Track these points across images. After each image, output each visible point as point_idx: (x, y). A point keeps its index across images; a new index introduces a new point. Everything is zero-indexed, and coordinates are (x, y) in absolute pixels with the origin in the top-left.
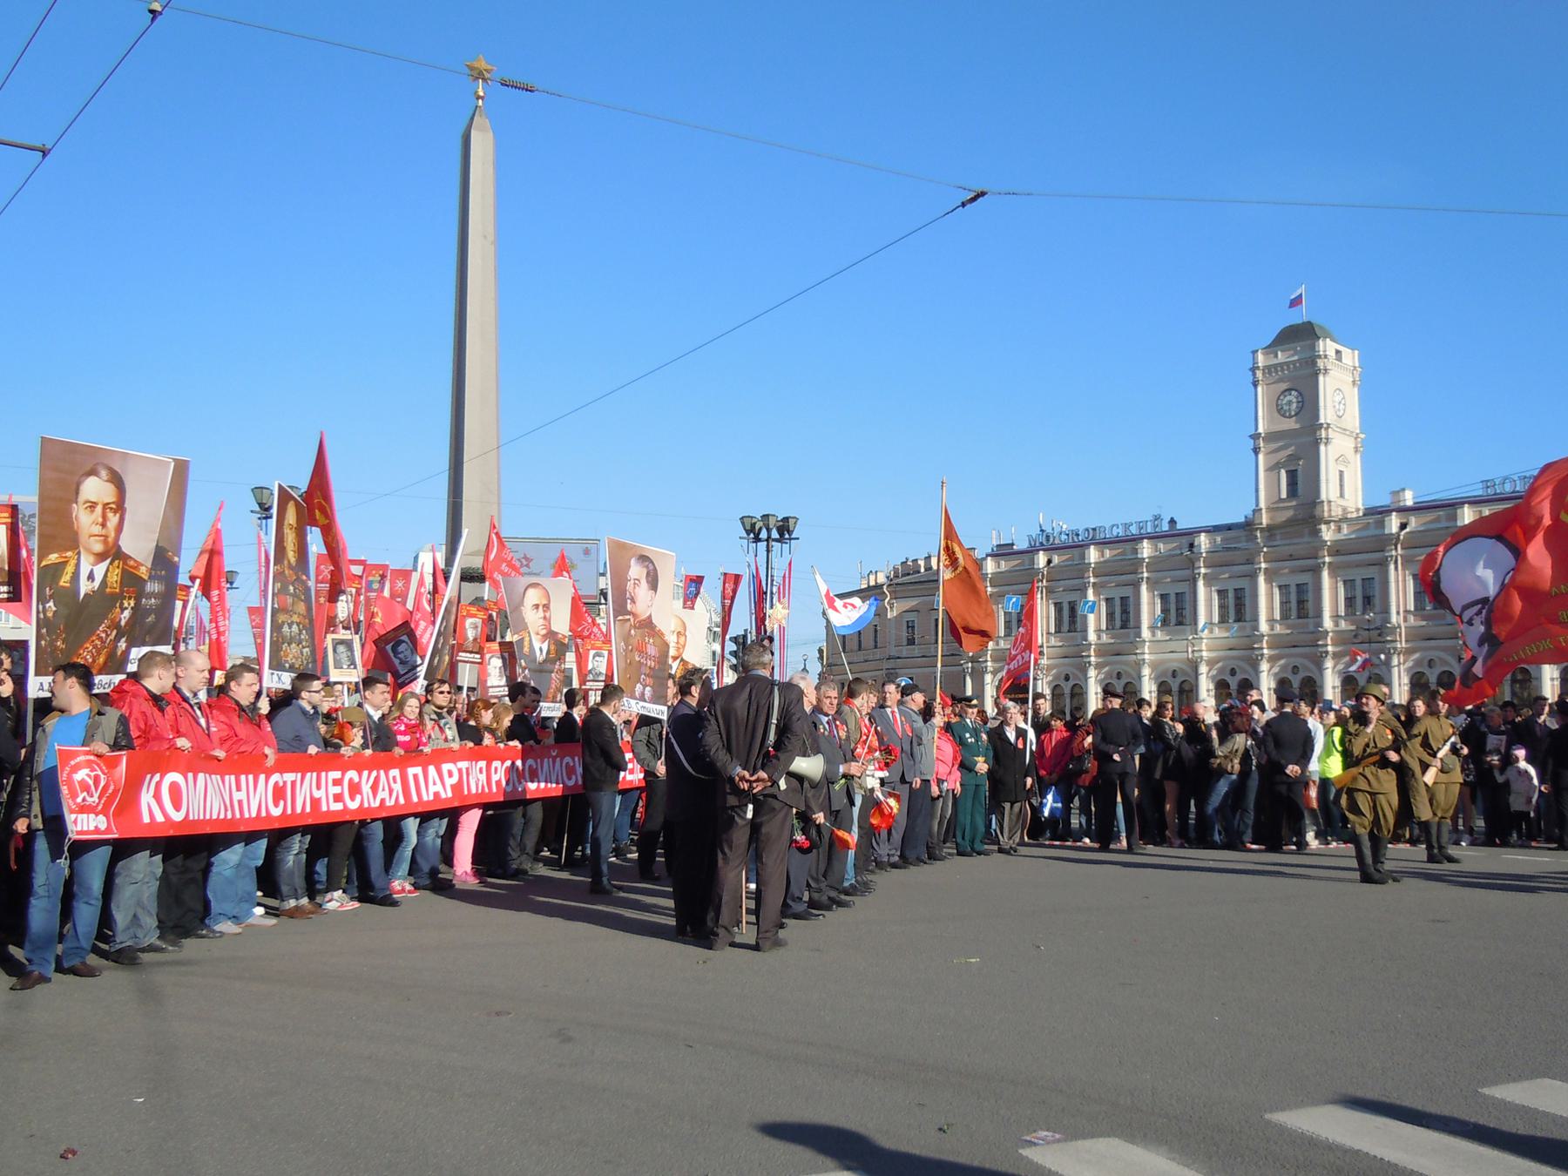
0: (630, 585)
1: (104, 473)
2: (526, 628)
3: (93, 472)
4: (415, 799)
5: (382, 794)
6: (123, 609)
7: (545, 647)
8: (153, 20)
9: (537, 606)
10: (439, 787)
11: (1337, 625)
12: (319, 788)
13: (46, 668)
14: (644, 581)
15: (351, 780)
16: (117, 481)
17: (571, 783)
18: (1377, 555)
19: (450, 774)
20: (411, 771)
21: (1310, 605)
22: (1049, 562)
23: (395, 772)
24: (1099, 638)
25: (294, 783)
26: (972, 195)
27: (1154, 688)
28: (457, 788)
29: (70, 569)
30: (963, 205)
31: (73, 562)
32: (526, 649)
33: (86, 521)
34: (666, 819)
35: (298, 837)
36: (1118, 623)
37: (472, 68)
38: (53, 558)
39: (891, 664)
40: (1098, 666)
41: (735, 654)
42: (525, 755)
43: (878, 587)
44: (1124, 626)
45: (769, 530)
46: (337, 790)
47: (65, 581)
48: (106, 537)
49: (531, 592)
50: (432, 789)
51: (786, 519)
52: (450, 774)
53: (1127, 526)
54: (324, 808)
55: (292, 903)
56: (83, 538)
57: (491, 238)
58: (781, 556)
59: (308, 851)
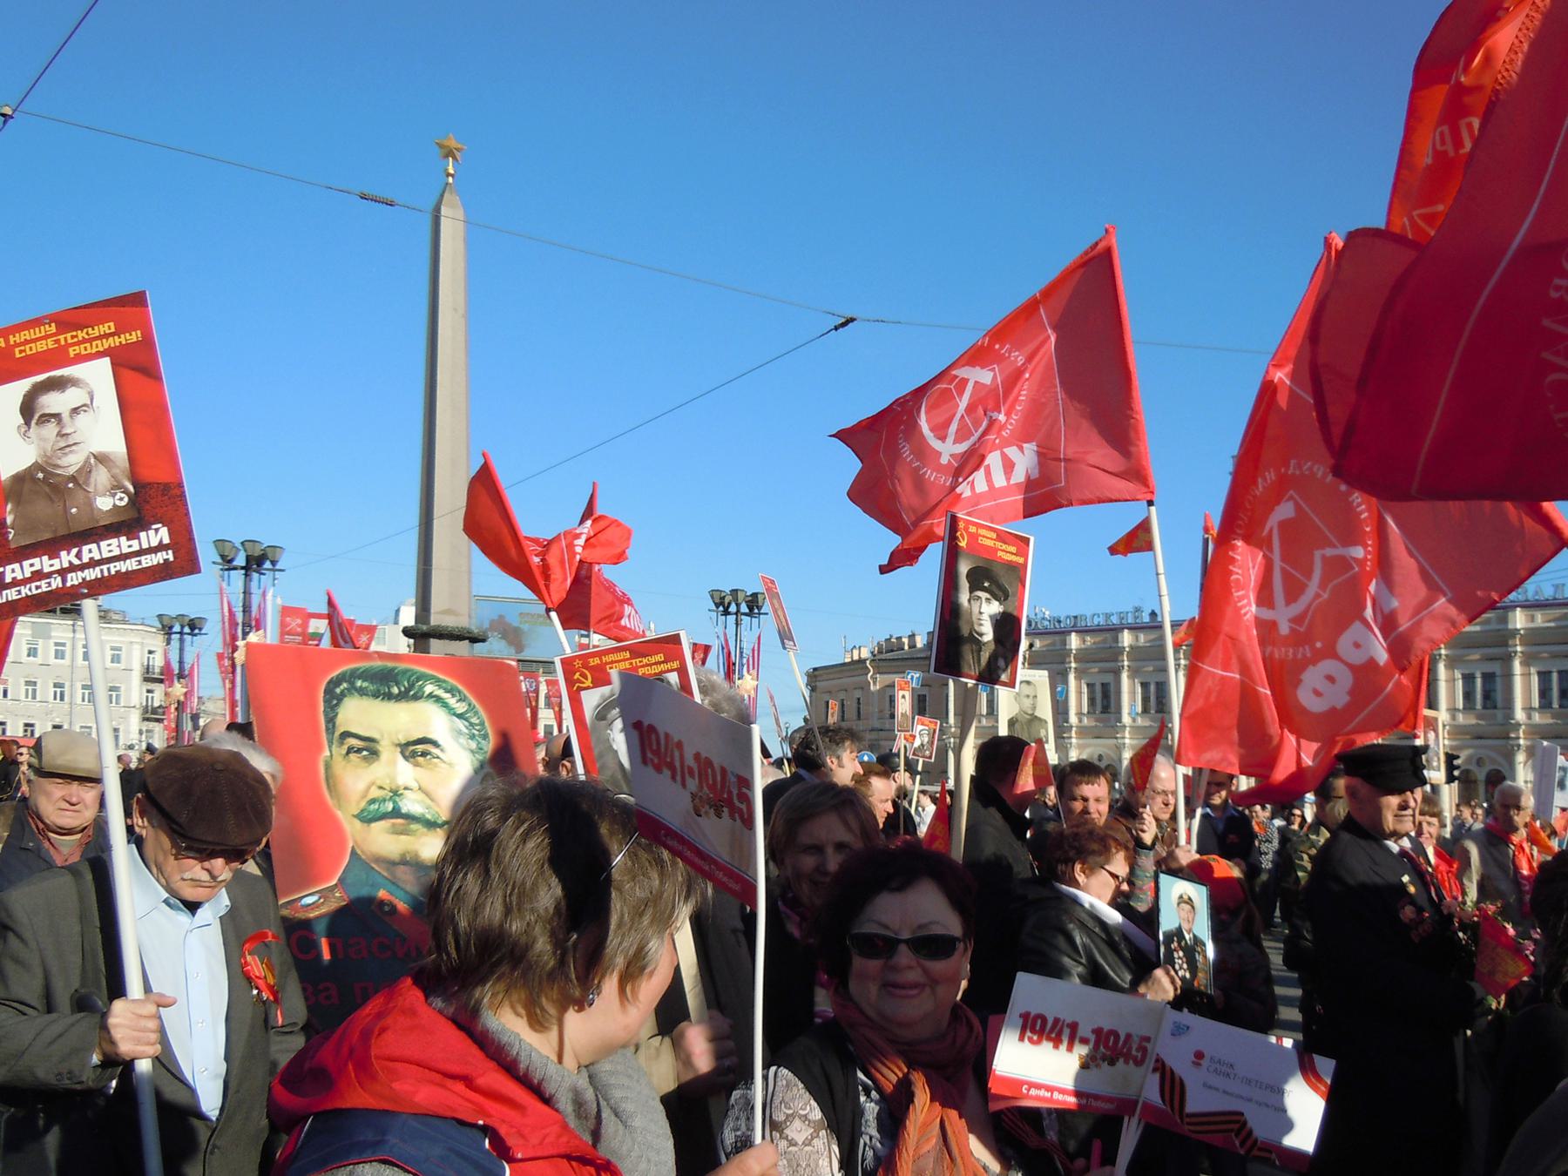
11: (1529, 717)
18: (1112, 665)
21: (1499, 696)
22: (1031, 646)
27: (1530, 777)
30: (836, 328)
36: (1099, 708)
37: (441, 146)
43: (862, 661)
51: (755, 595)
53: (1108, 616)
57: (461, 311)
58: (750, 630)
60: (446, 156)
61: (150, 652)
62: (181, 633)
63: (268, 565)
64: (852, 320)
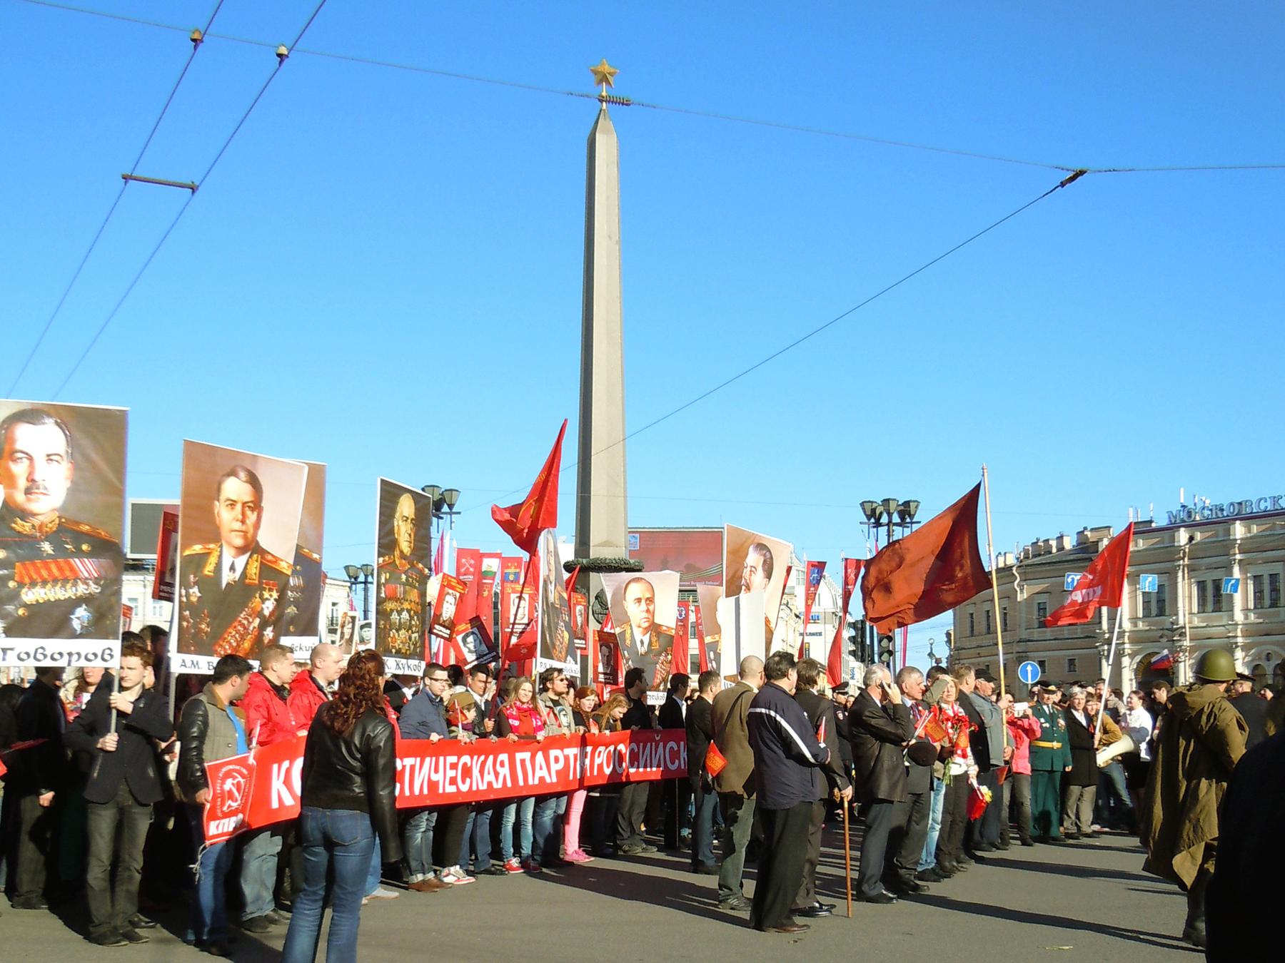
0: (746, 572)
1: (242, 475)
2: (628, 621)
3: (233, 473)
4: (521, 783)
5: (489, 777)
6: (263, 600)
7: (646, 639)
8: (195, 48)
9: (639, 600)
10: (544, 773)
12: (436, 771)
13: (188, 647)
14: (760, 570)
15: (465, 764)
16: (254, 481)
17: (673, 767)
18: (1169, 565)
19: (557, 760)
20: (519, 756)
22: (1191, 539)
23: (504, 757)
24: (1246, 617)
25: (412, 767)
26: (1071, 174)
28: (562, 774)
29: (213, 560)
30: (1063, 185)
31: (216, 554)
32: (628, 642)
33: (227, 518)
34: (716, 793)
35: (425, 815)
36: (1267, 602)
37: (595, 73)
38: (197, 548)
39: (1022, 647)
40: (1246, 648)
41: (853, 639)
42: (633, 739)
44: (1274, 604)
45: (890, 515)
46: (451, 773)
47: (209, 569)
48: (245, 532)
49: (633, 586)
50: (539, 773)
51: (907, 504)
52: (557, 760)
54: (441, 791)
55: (420, 877)
56: (225, 532)
59: (435, 829)
60: (600, 82)
61: (334, 604)
62: (366, 583)
63: (445, 508)
64: (1082, 173)
